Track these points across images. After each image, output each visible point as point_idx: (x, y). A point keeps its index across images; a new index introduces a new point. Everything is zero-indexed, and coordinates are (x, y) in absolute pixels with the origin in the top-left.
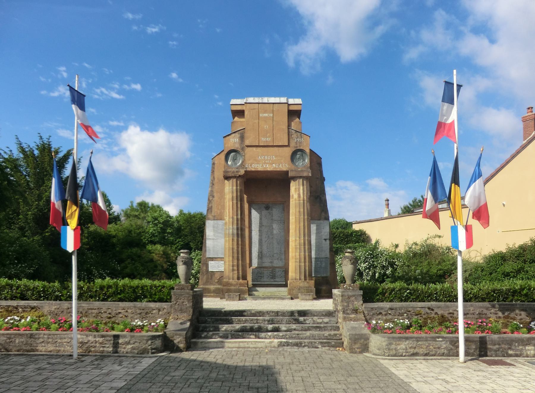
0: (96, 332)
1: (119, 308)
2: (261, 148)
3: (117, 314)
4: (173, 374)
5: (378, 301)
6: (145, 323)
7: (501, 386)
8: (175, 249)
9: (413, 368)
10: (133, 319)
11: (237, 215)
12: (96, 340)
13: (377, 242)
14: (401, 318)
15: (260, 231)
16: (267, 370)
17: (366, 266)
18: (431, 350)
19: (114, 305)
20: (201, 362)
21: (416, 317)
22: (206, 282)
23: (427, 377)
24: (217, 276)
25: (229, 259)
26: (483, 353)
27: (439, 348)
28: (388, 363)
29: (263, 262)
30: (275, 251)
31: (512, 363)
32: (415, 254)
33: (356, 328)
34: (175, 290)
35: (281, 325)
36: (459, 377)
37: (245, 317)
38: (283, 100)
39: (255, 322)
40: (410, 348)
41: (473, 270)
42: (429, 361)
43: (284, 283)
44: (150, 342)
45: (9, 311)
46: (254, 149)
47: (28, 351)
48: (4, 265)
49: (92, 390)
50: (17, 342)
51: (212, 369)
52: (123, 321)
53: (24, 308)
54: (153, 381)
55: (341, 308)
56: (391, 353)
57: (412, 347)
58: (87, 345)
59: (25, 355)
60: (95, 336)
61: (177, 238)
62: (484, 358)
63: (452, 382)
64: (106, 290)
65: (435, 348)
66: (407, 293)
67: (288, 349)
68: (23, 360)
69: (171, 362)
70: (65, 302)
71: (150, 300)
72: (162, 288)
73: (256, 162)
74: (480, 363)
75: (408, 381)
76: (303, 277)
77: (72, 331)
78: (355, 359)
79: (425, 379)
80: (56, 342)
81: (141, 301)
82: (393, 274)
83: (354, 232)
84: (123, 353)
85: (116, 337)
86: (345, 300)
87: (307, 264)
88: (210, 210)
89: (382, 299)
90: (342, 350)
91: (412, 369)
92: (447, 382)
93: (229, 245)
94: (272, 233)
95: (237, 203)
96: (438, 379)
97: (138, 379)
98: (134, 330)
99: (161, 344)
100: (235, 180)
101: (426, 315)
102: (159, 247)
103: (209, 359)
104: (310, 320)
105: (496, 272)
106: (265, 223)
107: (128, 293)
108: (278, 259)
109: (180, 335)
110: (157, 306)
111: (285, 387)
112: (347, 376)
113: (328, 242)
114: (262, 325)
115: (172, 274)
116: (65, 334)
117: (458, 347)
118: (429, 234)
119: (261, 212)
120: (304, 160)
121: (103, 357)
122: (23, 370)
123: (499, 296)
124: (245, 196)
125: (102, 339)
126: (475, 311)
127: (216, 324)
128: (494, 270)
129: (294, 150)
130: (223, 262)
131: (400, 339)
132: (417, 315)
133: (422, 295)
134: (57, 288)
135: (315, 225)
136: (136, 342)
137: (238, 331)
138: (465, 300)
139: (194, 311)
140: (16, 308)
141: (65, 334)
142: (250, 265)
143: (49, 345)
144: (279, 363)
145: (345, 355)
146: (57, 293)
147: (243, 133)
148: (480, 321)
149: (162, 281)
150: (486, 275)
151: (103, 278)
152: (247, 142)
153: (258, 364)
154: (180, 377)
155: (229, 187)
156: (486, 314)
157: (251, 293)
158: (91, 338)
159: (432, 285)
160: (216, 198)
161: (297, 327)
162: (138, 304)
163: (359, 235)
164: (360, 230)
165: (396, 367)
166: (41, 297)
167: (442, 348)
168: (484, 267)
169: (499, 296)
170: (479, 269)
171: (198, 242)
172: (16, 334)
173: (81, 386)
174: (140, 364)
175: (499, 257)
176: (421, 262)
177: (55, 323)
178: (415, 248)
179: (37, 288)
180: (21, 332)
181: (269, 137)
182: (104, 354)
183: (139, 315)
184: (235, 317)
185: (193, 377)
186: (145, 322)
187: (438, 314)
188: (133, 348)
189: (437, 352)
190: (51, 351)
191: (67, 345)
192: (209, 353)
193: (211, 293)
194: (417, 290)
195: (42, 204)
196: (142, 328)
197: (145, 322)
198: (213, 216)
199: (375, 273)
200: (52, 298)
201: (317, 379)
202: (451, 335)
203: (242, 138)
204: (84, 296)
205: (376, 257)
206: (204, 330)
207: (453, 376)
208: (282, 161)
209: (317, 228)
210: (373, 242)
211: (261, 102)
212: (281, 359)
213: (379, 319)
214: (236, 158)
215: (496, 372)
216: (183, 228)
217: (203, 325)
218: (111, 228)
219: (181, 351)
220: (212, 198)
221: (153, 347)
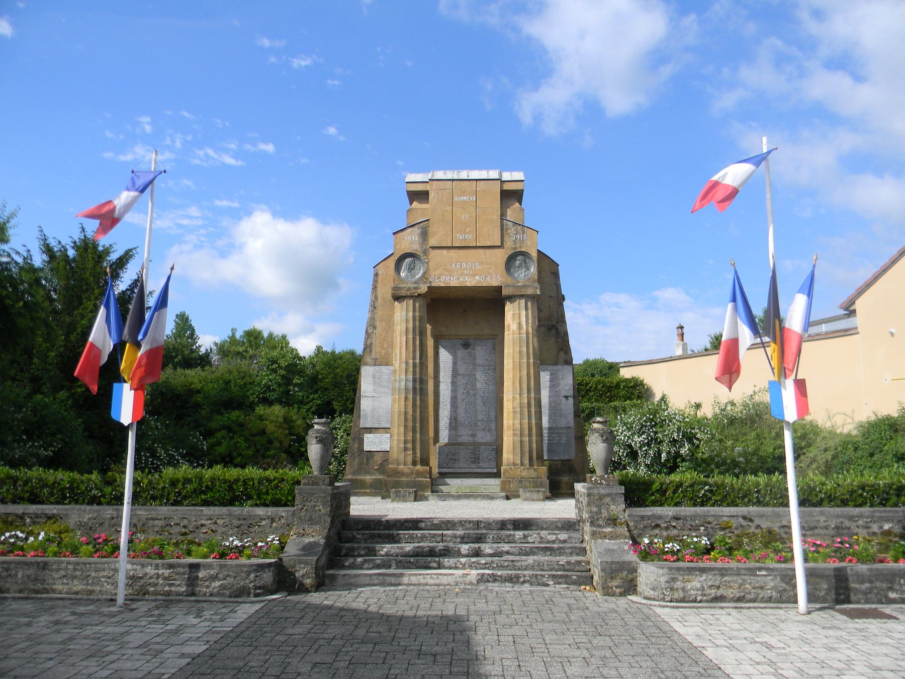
0: (160, 559)
1: (202, 517)
3: (197, 528)
4: (290, 631)
5: (654, 503)
6: (246, 542)
7: (864, 654)
8: (307, 412)
9: (712, 622)
10: (225, 536)
11: (414, 358)
12: (157, 573)
13: (663, 399)
14: (694, 534)
15: (453, 383)
16: (455, 623)
19: (194, 513)
20: (342, 609)
21: (722, 533)
22: (357, 470)
23: (736, 638)
24: (378, 459)
25: (398, 430)
26: (842, 597)
27: (762, 588)
28: (668, 614)
30: (480, 417)
31: (894, 614)
32: (732, 421)
33: (613, 550)
34: (301, 486)
35: (484, 545)
36: (792, 639)
37: (422, 532)
38: (494, 174)
39: (439, 539)
40: (710, 587)
41: (839, 449)
42: (744, 611)
43: (495, 471)
44: (252, 576)
45: (9, 522)
46: (445, 252)
47: (37, 592)
48: (2, 443)
49: (149, 658)
50: (20, 576)
51: (359, 622)
52: (208, 540)
53: (36, 516)
54: (254, 644)
55: (587, 516)
56: (676, 596)
57: (712, 586)
59: (33, 598)
60: (157, 567)
61: (311, 393)
62: (845, 606)
63: (779, 648)
64: (180, 486)
65: (754, 588)
66: (705, 491)
67: (495, 587)
68: (28, 606)
69: (289, 610)
70: (107, 507)
72: (279, 482)
74: (836, 615)
75: (700, 645)
76: (527, 462)
77: (117, 557)
78: (612, 606)
79: (731, 642)
80: (89, 576)
81: (241, 505)
82: (693, 455)
83: (623, 381)
84: (205, 595)
85: (195, 567)
86: (594, 503)
87: (534, 438)
88: (368, 350)
89: (661, 501)
90: (589, 591)
91: (711, 624)
92: (769, 647)
93: (399, 406)
94: (474, 388)
95: (414, 339)
96: (756, 642)
97: (229, 640)
98: (227, 554)
99: (272, 579)
101: (740, 529)
102: (277, 410)
103: (354, 605)
105: (881, 452)
106: (461, 369)
107: (219, 491)
109: (306, 563)
110: (269, 514)
111: (483, 653)
112: (592, 635)
113: (571, 400)
114: (451, 545)
115: (298, 456)
116: (105, 563)
117: (795, 586)
118: (755, 386)
119: (455, 352)
120: (528, 269)
121: (168, 601)
122: (29, 625)
123: (872, 496)
124: (429, 327)
125: (168, 571)
126: (829, 523)
127: (371, 543)
128: (877, 448)
129: (510, 253)
130: (388, 435)
131: (691, 570)
132: (723, 529)
133: (733, 494)
134: (96, 484)
135: (548, 373)
136: (228, 576)
137: (407, 555)
138: (802, 503)
139: (332, 522)
140: (21, 517)
141: (105, 563)
142: (436, 439)
143: (75, 582)
144: (476, 611)
145: (595, 598)
146: (95, 492)
148: (839, 540)
150: (863, 456)
151: (175, 464)
153: (439, 613)
154: (301, 637)
156: (849, 528)
157: (435, 488)
158: (149, 570)
159: (751, 478)
160: (379, 329)
161: (512, 549)
162: (236, 510)
163: (631, 387)
164: (633, 378)
165: (682, 620)
166: (65, 498)
167: (767, 587)
168: (859, 442)
169: (872, 496)
170: (850, 446)
171: (347, 400)
172: (18, 563)
173: (130, 652)
174: (233, 615)
175: (885, 425)
176: (744, 434)
177: (87, 544)
178: (732, 410)
179: (59, 484)
180: (29, 558)
181: (469, 233)
182: (171, 598)
183: (236, 529)
184: (405, 530)
185: (325, 635)
186: (247, 541)
187: (761, 528)
188: (222, 587)
189: (758, 594)
190: (77, 593)
191: (106, 582)
192: (356, 595)
194: (723, 485)
195: (73, 339)
196: (240, 551)
197: (247, 541)
199: (659, 453)
200: (84, 500)
201: (540, 640)
202: (783, 565)
203: (424, 235)
204: (142, 497)
205: (662, 424)
206: (350, 553)
207: (781, 638)
208: (491, 271)
209: (550, 378)
210: (658, 397)
211: (456, 178)
212: (481, 605)
213: (656, 536)
214: (414, 267)
215: (860, 630)
216: (320, 377)
217: (348, 545)
218: (193, 375)
219: (307, 591)
221: (258, 585)
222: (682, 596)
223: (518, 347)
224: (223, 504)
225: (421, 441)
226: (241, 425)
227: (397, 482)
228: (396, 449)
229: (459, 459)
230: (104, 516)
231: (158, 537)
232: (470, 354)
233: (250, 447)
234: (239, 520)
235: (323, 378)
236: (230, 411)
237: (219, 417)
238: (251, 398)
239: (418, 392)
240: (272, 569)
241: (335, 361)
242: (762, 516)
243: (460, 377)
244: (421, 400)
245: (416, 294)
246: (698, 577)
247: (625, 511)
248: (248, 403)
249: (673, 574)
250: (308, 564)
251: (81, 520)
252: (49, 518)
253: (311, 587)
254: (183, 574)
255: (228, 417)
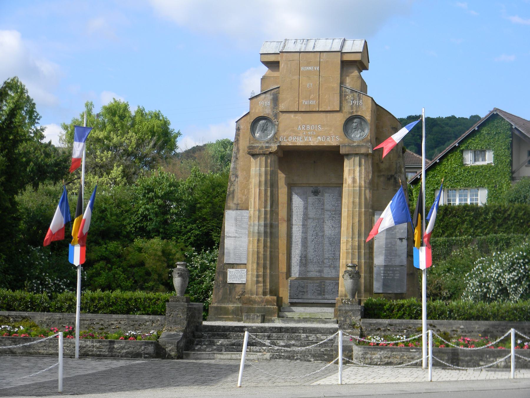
2: (302, 114)
3: (109, 326)
8: (185, 242)
11: (265, 207)
15: (304, 225)
17: (512, 278)
18: (405, 360)
25: (252, 266)
29: (308, 272)
30: (326, 256)
40: (385, 357)
44: (143, 347)
45: (4, 320)
46: (292, 115)
56: (367, 361)
57: (386, 357)
58: (85, 349)
64: (97, 301)
65: (408, 358)
71: (144, 312)
72: (157, 300)
73: (294, 134)
81: (134, 314)
86: (342, 315)
95: (266, 190)
99: (153, 350)
100: (264, 158)
102: (156, 243)
104: (313, 336)
106: (312, 213)
107: (120, 305)
108: (330, 266)
109: (172, 343)
110: (151, 318)
119: (307, 198)
136: (130, 347)
139: (188, 324)
140: (7, 317)
143: (50, 349)
147: (277, 94)
149: (157, 294)
152: (282, 107)
155: (256, 168)
161: (296, 343)
162: (132, 316)
183: (132, 327)
187: (440, 331)
191: (66, 349)
193: (229, 315)
198: (235, 204)
200: (39, 309)
203: (275, 100)
208: (331, 132)
214: (267, 128)
216: (198, 205)
220: (234, 179)
222: (369, 362)
223: (352, 199)
224: (122, 313)
225: (271, 276)
226: (119, 256)
227: (250, 308)
228: (250, 282)
229: (307, 291)
230: (55, 318)
231: (87, 331)
232: (319, 200)
233: (128, 278)
234: (133, 321)
235: (200, 208)
236: (107, 241)
237: (97, 248)
238: (129, 229)
239: (269, 235)
240: (153, 345)
241: (214, 189)
242: (441, 324)
243: (310, 221)
244: (271, 242)
245: (268, 153)
246: (379, 352)
247: (360, 320)
248: (125, 233)
249: (366, 350)
250: (173, 344)
251: (42, 320)
252: (24, 318)
253: (175, 357)
254: (106, 346)
255: (106, 248)
